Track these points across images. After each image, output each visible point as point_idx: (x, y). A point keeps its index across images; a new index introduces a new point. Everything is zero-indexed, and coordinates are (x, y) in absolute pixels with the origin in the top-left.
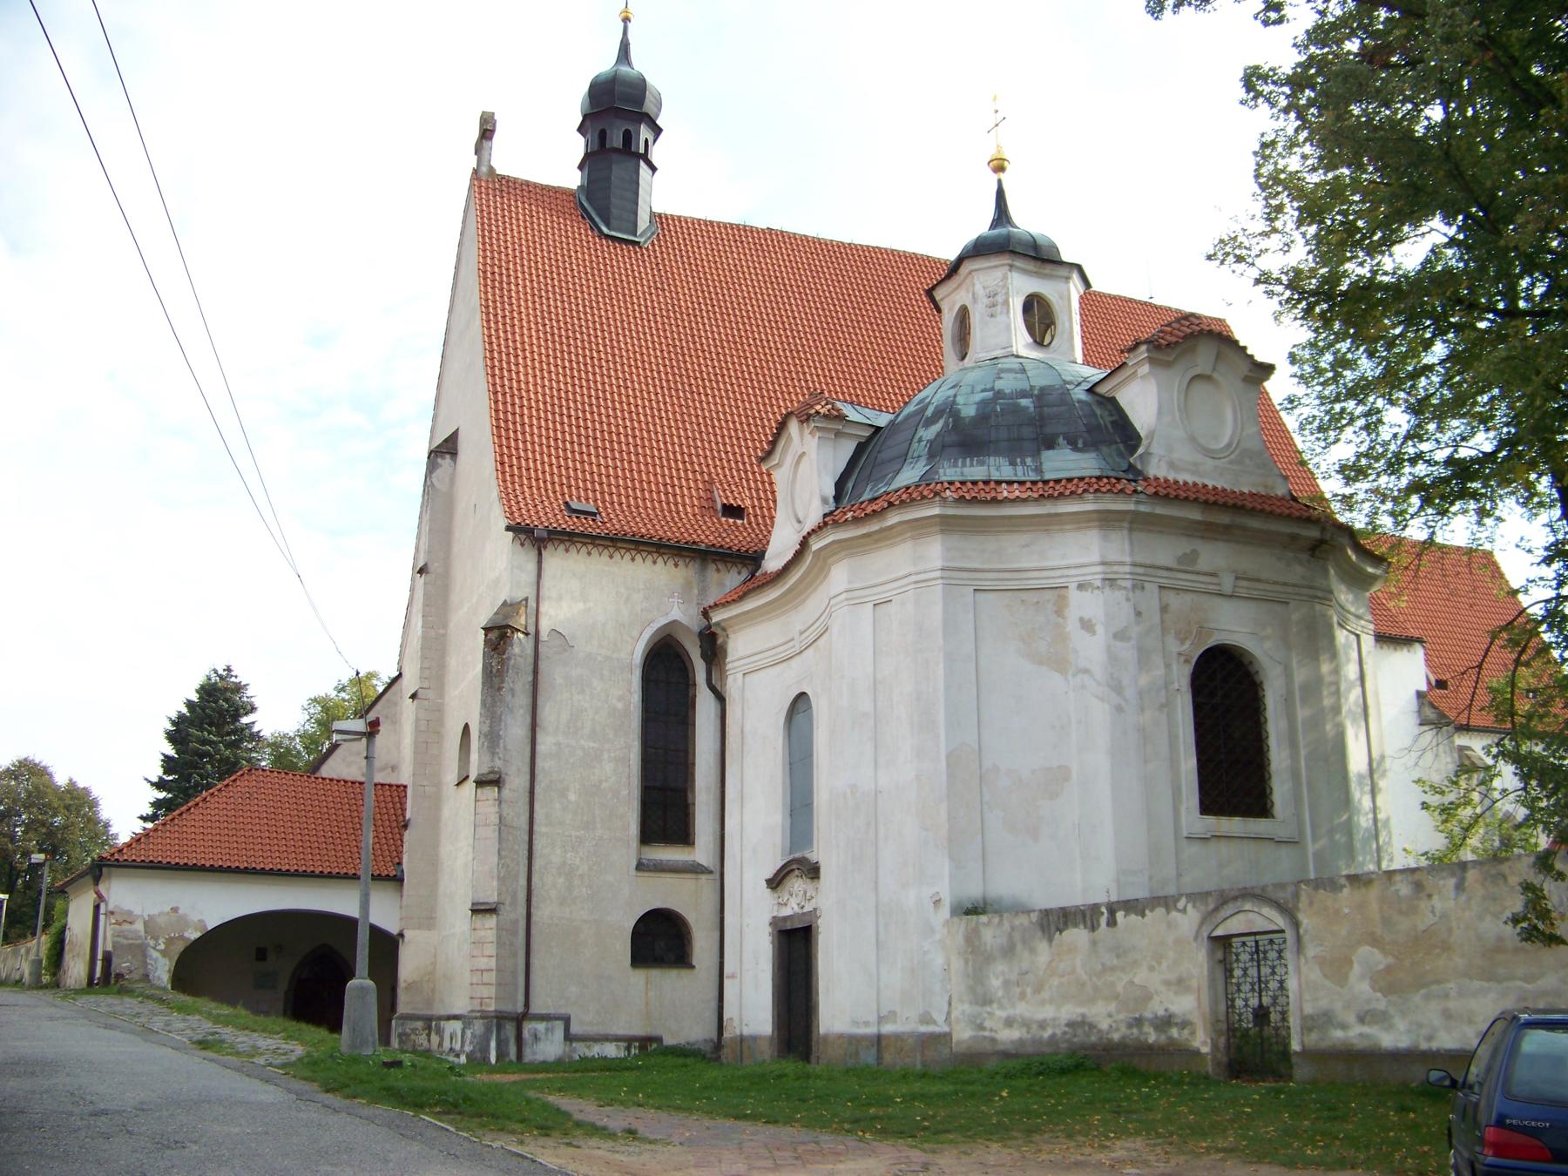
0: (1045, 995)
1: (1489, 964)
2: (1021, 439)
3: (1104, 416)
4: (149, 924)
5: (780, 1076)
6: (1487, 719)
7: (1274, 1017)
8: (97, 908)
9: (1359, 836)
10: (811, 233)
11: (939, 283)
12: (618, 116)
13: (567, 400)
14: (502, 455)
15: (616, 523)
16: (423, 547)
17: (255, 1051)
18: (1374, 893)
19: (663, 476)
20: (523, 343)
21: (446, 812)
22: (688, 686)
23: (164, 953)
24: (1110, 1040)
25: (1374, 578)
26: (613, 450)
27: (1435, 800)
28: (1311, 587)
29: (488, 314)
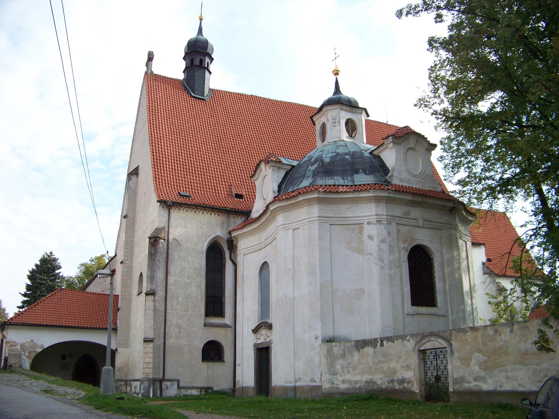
0: (357, 371)
1: (523, 358)
2: (346, 170)
3: (376, 163)
4: (22, 346)
5: (260, 402)
6: (510, 272)
7: (443, 379)
8: (2, 340)
9: (467, 313)
10: (267, 97)
11: (315, 114)
12: (198, 54)
13: (179, 155)
14: (155, 175)
15: (197, 200)
16: (125, 208)
17: (66, 394)
18: (479, 334)
19: (214, 183)
20: (163, 134)
21: (134, 305)
22: (222, 259)
23: (28, 357)
24: (381, 388)
25: (471, 221)
26: (195, 174)
27: (494, 301)
28: (450, 224)
29: (150, 124)
